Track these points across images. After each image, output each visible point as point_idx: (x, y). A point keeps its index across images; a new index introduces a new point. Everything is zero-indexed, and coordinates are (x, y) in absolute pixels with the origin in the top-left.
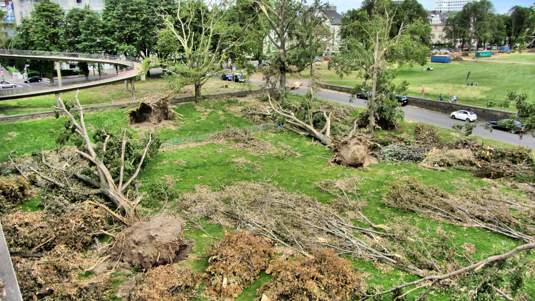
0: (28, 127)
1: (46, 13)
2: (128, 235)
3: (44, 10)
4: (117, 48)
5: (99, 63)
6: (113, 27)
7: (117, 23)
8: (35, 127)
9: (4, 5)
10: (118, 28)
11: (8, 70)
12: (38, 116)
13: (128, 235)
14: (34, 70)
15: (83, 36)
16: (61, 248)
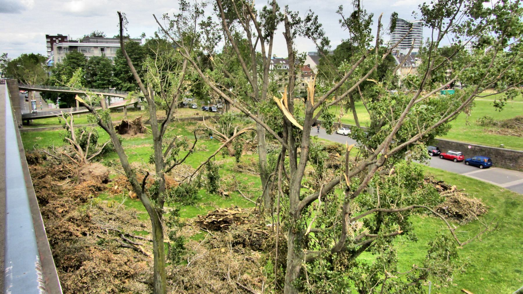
0: (49, 134)
1: (73, 60)
2: (79, 171)
3: (73, 58)
4: (122, 86)
5: (109, 96)
6: (120, 70)
7: (123, 68)
8: (54, 134)
9: (50, 50)
10: (124, 71)
11: (46, 102)
12: (57, 128)
13: (79, 171)
14: (65, 102)
15: (98, 77)
16: (49, 177)
